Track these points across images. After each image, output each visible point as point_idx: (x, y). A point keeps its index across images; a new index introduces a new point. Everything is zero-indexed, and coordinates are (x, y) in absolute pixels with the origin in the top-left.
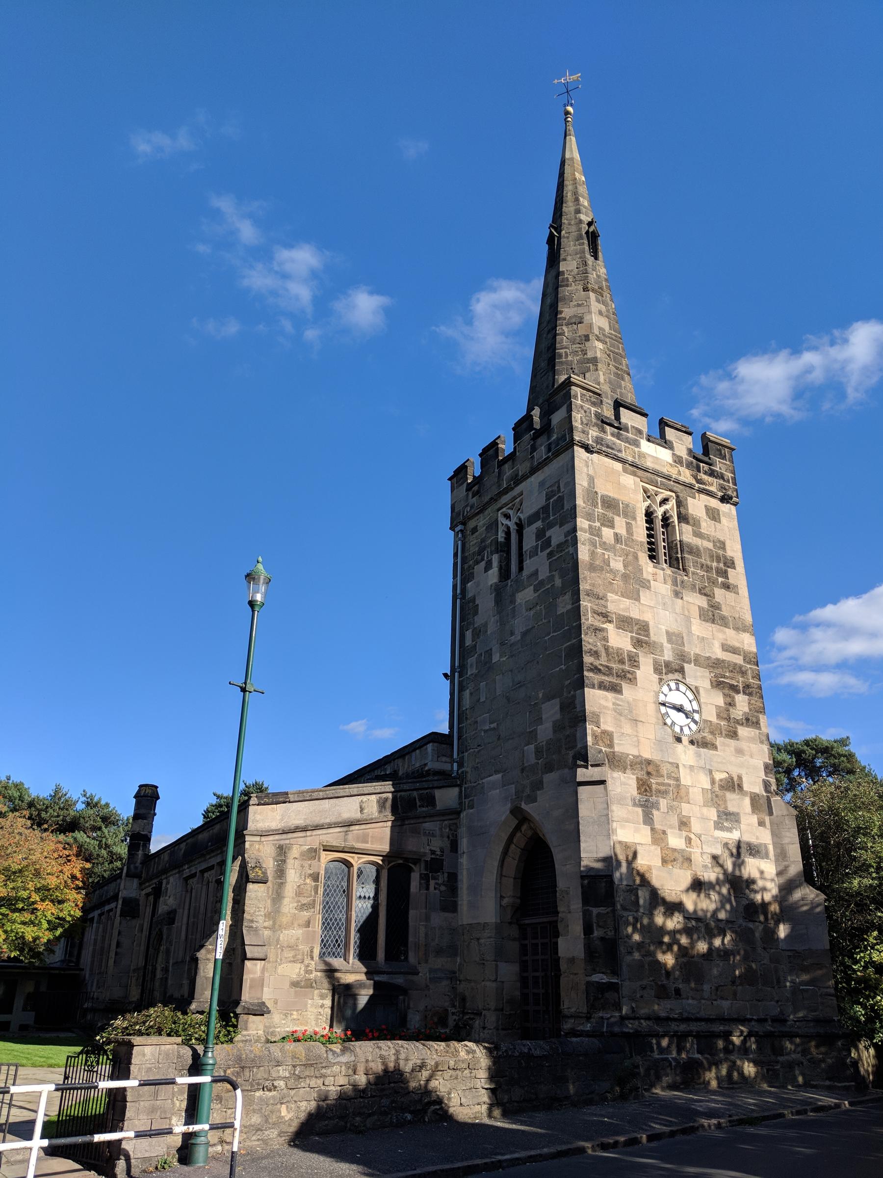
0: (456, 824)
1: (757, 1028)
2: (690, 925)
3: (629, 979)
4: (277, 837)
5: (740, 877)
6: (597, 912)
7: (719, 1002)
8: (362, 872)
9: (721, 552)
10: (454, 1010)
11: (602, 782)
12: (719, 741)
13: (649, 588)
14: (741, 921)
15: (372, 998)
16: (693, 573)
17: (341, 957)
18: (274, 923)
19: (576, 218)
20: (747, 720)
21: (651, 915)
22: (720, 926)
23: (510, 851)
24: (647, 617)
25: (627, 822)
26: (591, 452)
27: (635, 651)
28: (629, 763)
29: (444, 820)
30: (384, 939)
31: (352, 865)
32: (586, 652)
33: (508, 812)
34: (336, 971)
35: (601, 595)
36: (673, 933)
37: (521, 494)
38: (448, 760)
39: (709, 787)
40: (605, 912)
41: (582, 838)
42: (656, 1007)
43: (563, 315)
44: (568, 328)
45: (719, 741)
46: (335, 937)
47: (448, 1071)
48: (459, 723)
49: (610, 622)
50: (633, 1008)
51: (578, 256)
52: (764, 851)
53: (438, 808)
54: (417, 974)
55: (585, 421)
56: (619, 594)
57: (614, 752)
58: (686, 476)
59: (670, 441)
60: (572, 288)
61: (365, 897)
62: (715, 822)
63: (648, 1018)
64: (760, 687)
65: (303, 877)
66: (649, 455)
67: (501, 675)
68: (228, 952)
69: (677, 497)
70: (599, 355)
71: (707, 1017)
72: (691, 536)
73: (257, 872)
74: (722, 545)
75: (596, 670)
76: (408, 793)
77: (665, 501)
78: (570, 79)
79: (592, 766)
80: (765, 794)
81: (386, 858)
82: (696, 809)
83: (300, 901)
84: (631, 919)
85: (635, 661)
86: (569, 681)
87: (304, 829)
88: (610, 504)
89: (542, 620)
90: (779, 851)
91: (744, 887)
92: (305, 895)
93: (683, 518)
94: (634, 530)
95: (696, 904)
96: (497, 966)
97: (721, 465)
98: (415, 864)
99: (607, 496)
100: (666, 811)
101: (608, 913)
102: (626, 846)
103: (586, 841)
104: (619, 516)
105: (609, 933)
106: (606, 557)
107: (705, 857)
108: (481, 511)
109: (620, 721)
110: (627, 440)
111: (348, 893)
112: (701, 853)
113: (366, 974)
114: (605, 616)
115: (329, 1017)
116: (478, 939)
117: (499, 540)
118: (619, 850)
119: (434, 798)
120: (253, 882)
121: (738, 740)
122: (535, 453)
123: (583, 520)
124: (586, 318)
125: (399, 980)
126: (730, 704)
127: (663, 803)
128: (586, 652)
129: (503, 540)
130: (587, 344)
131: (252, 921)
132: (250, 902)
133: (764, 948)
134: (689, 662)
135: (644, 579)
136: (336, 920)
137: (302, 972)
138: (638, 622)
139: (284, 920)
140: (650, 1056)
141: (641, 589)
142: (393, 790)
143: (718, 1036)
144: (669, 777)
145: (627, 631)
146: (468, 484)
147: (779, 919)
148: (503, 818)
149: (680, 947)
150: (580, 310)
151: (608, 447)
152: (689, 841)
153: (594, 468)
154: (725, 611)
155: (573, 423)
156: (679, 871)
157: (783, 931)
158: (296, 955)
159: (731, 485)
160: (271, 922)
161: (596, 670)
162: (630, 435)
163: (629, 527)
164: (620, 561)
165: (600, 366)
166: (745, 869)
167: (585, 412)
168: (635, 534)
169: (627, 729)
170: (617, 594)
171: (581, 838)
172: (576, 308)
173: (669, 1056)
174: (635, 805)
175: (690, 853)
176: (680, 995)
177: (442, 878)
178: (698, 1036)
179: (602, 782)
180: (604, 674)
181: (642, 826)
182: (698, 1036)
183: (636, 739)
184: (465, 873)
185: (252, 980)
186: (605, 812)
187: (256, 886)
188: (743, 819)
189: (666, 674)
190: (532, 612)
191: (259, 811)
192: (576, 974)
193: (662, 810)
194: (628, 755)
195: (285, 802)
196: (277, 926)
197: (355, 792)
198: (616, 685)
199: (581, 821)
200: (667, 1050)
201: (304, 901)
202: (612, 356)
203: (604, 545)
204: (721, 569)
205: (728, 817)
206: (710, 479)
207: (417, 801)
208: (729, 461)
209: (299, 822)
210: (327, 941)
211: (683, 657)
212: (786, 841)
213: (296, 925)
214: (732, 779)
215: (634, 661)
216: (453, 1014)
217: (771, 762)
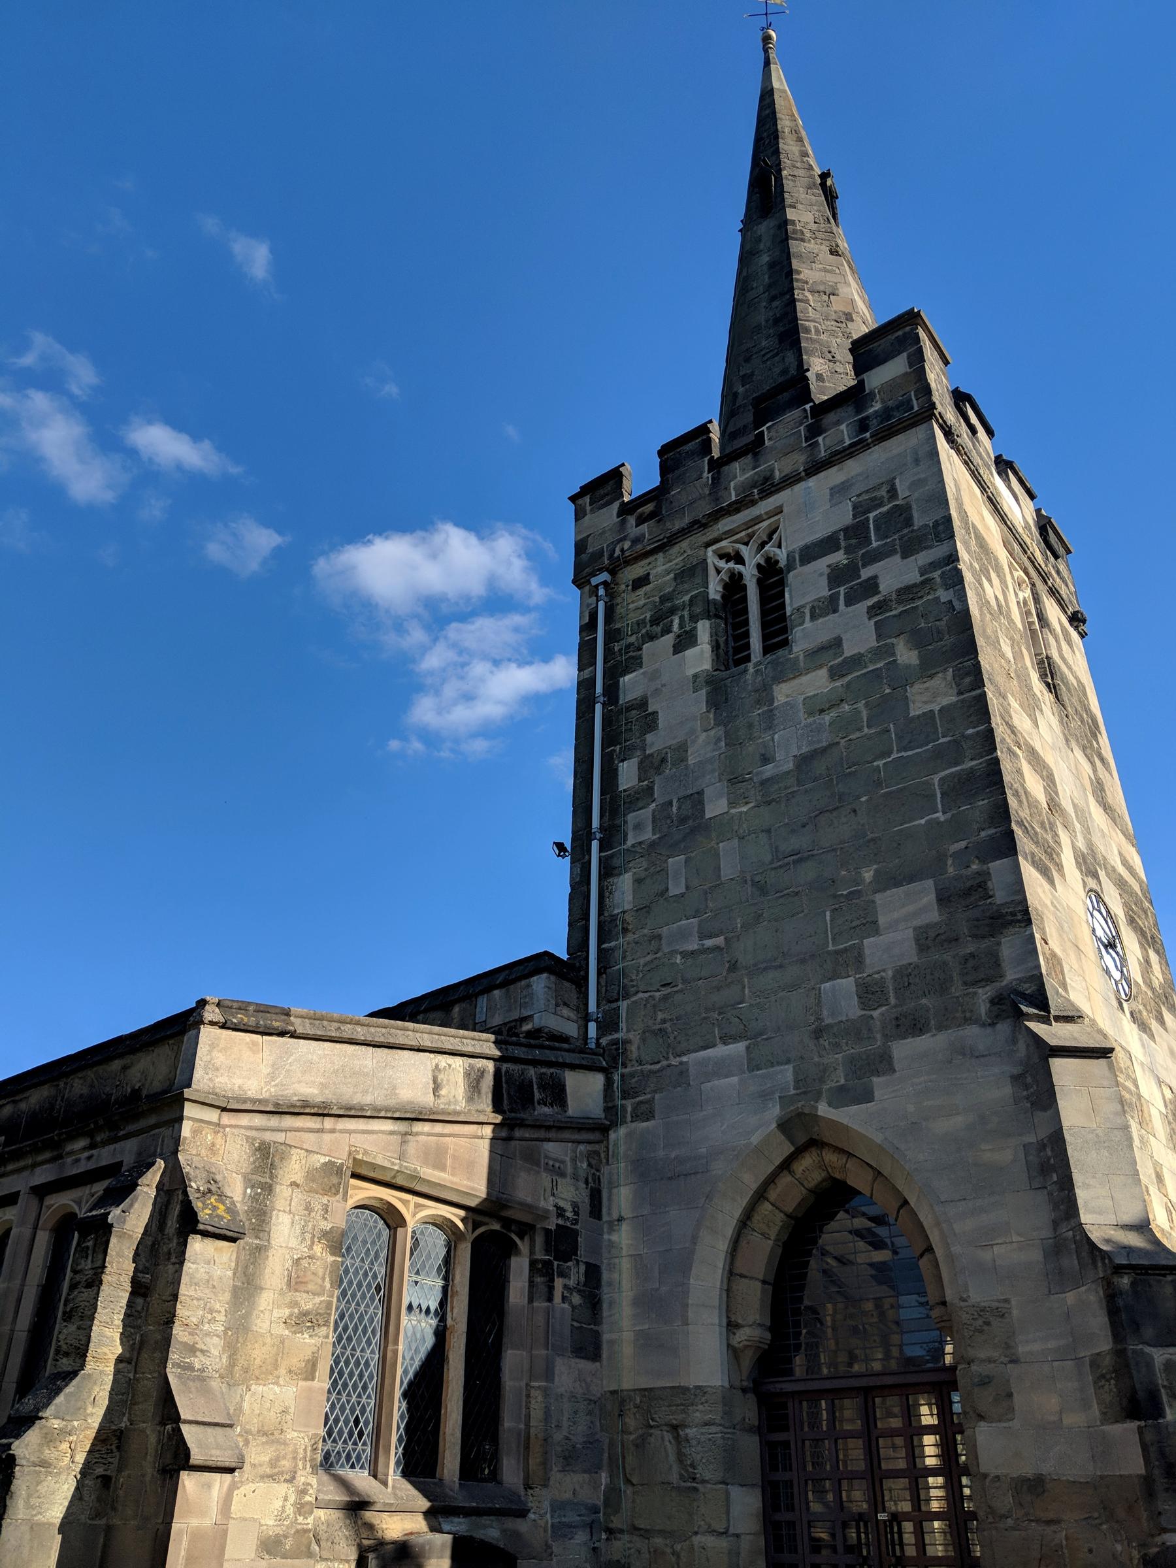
4: (258, 1120)
23: (756, 1217)
29: (579, 1142)
30: (460, 1422)
31: (402, 1222)
33: (774, 1125)
37: (779, 511)
41: (1077, 1177)
43: (801, 276)
46: (353, 1410)
48: (600, 941)
53: (570, 1112)
65: (308, 1236)
67: (736, 841)
68: (104, 1441)
73: (215, 1208)
79: (1058, 1019)
81: (475, 1214)
83: (295, 1304)
86: (963, 844)
87: (322, 1112)
89: (860, 729)
92: (311, 1287)
103: (1087, 1186)
108: (661, 548)
111: (387, 1292)
113: (428, 1514)
120: (205, 1234)
122: (820, 439)
129: (718, 597)
136: (357, 1363)
137: (290, 1510)
139: (258, 1353)
146: (623, 504)
148: (755, 1139)
158: (278, 1459)
177: (576, 1274)
184: (626, 1265)
185: (197, 1536)
186: (1119, 1121)
190: (827, 718)
191: (222, 1044)
192: (1049, 1522)
195: (282, 1034)
197: (426, 1041)
207: (536, 1091)
209: (307, 1089)
210: (337, 1420)
213: (282, 1371)
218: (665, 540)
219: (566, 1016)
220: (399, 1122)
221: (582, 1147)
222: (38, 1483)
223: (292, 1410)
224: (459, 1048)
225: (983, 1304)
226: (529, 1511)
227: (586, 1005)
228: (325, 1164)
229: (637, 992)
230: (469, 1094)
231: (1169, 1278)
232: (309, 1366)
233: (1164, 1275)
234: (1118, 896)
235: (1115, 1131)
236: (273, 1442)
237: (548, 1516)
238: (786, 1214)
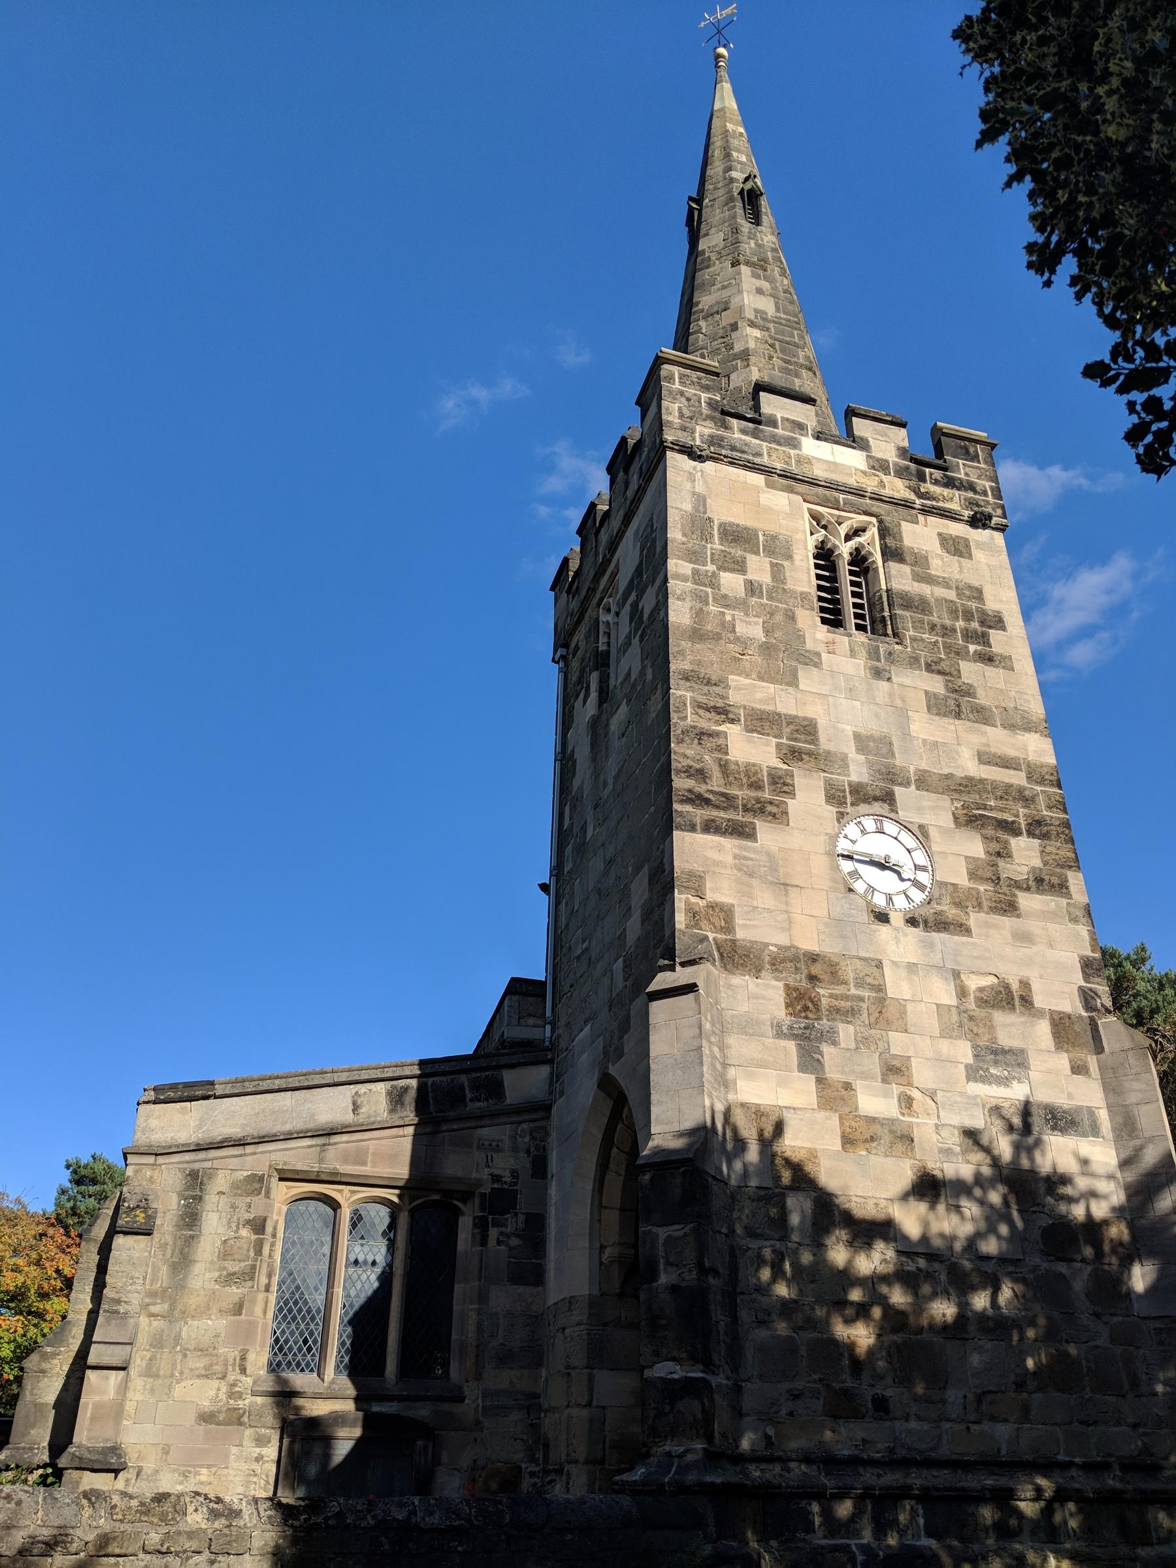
1: (1081, 1481)
2: (911, 1267)
3: (761, 1377)
4: (188, 1157)
5: (1033, 1172)
6: (664, 1236)
7: (986, 1426)
8: (360, 1218)
9: (973, 605)
10: (533, 1468)
11: (691, 988)
12: (974, 919)
13: (818, 665)
14: (1036, 1260)
15: (359, 1442)
16: (913, 639)
17: (312, 1370)
18: (172, 1308)
19: (725, 179)
20: (1039, 881)
21: (819, 1246)
22: (985, 1268)
24: (813, 711)
25: (761, 1066)
26: (700, 458)
27: (785, 767)
28: (767, 958)
29: (521, 1122)
32: (678, 772)
34: (294, 1394)
35: (714, 678)
36: (872, 1283)
38: (539, 1022)
39: (954, 1001)
40: (681, 1233)
41: (654, 1097)
42: (828, 1435)
44: (706, 321)
45: (974, 919)
46: (301, 1334)
47: (141, 1556)
49: (732, 721)
50: (767, 1437)
51: (726, 224)
52: (1087, 1122)
53: (508, 1101)
54: (461, 1399)
55: (686, 412)
56: (754, 676)
57: (734, 941)
58: (897, 488)
59: (862, 439)
60: (715, 268)
61: (365, 1262)
62: (967, 1067)
63: (807, 1460)
64: (1067, 824)
65: (234, 1225)
66: (819, 460)
69: (880, 522)
70: (752, 345)
71: (954, 1457)
72: (910, 581)
73: (136, 1216)
74: (978, 594)
75: (700, 800)
76: (449, 1078)
77: (858, 532)
78: (721, 15)
79: (683, 964)
80: (1085, 1014)
81: (408, 1189)
82: (924, 1044)
83: (225, 1268)
84: (767, 1253)
85: (784, 784)
87: (240, 1143)
88: (736, 536)
90: (1121, 1120)
91: (1042, 1190)
92: (236, 1257)
93: (892, 553)
94: (788, 574)
95: (926, 1224)
96: (591, 1378)
97: (967, 469)
98: (464, 1201)
99: (731, 524)
100: (853, 1046)
101: (685, 1234)
102: (759, 1113)
104: (757, 553)
105: (687, 1276)
106: (728, 618)
107: (945, 1133)
109: (750, 886)
110: (774, 439)
112: (937, 1126)
113: (357, 1400)
114: (724, 713)
115: (272, 1480)
116: (564, 1329)
117: (600, 649)
118: (739, 1118)
119: (500, 1084)
120: (125, 1233)
121: (1018, 916)
123: (680, 562)
124: (735, 302)
125: (423, 1412)
126: (999, 854)
127: (846, 1032)
128: (678, 772)
130: (734, 335)
131: (118, 1302)
132: (117, 1268)
133: (1097, 1315)
134: (907, 784)
135: (808, 651)
137: (223, 1396)
138: (791, 720)
140: (804, 1540)
141: (800, 666)
142: (418, 1072)
143: (980, 1498)
144: (859, 984)
145: (768, 735)
147: (1129, 1255)
149: (888, 1308)
150: (725, 294)
151: (733, 448)
152: (907, 1102)
153: (706, 482)
154: (983, 698)
155: (664, 417)
156: (882, 1159)
157: (1140, 1278)
158: (211, 1365)
159: (990, 499)
160: (166, 1306)
161: (700, 800)
162: (780, 431)
163: (777, 572)
164: (756, 624)
165: (753, 359)
166: (1043, 1154)
167: (688, 400)
168: (789, 581)
169: (765, 898)
170: (748, 676)
171: (652, 1097)
172: (720, 293)
173: (853, 1542)
174: (780, 1034)
175: (910, 1125)
176: (887, 1411)
177: (513, 1223)
178: (926, 1498)
179: (691, 988)
180: (717, 807)
181: (797, 1074)
182: (926, 1498)
183: (784, 916)
185: (98, 1406)
186: (696, 1044)
187: (131, 1239)
188: (1035, 1061)
189: (852, 804)
193: (842, 1046)
194: (766, 945)
196: (177, 1313)
198: (743, 825)
199: (652, 1066)
200: (849, 1527)
201: (234, 1267)
202: (777, 346)
203: (724, 601)
204: (976, 632)
205: (1000, 1057)
206: (946, 492)
208: (986, 462)
209: (233, 1130)
210: (286, 1341)
211: (892, 776)
212: (1132, 1098)
213: (214, 1311)
214: (1007, 987)
215: (782, 784)
216: (532, 1474)
217: (1097, 955)
220: (315, 1139)
221: (525, 1126)
222: (38, 1382)
223: (223, 1335)
224: (357, 1078)
226: (465, 1398)
228: (248, 1176)
230: (390, 1107)
232: (237, 1307)
235: (691, 1053)
236: (207, 1355)
237: (480, 1400)
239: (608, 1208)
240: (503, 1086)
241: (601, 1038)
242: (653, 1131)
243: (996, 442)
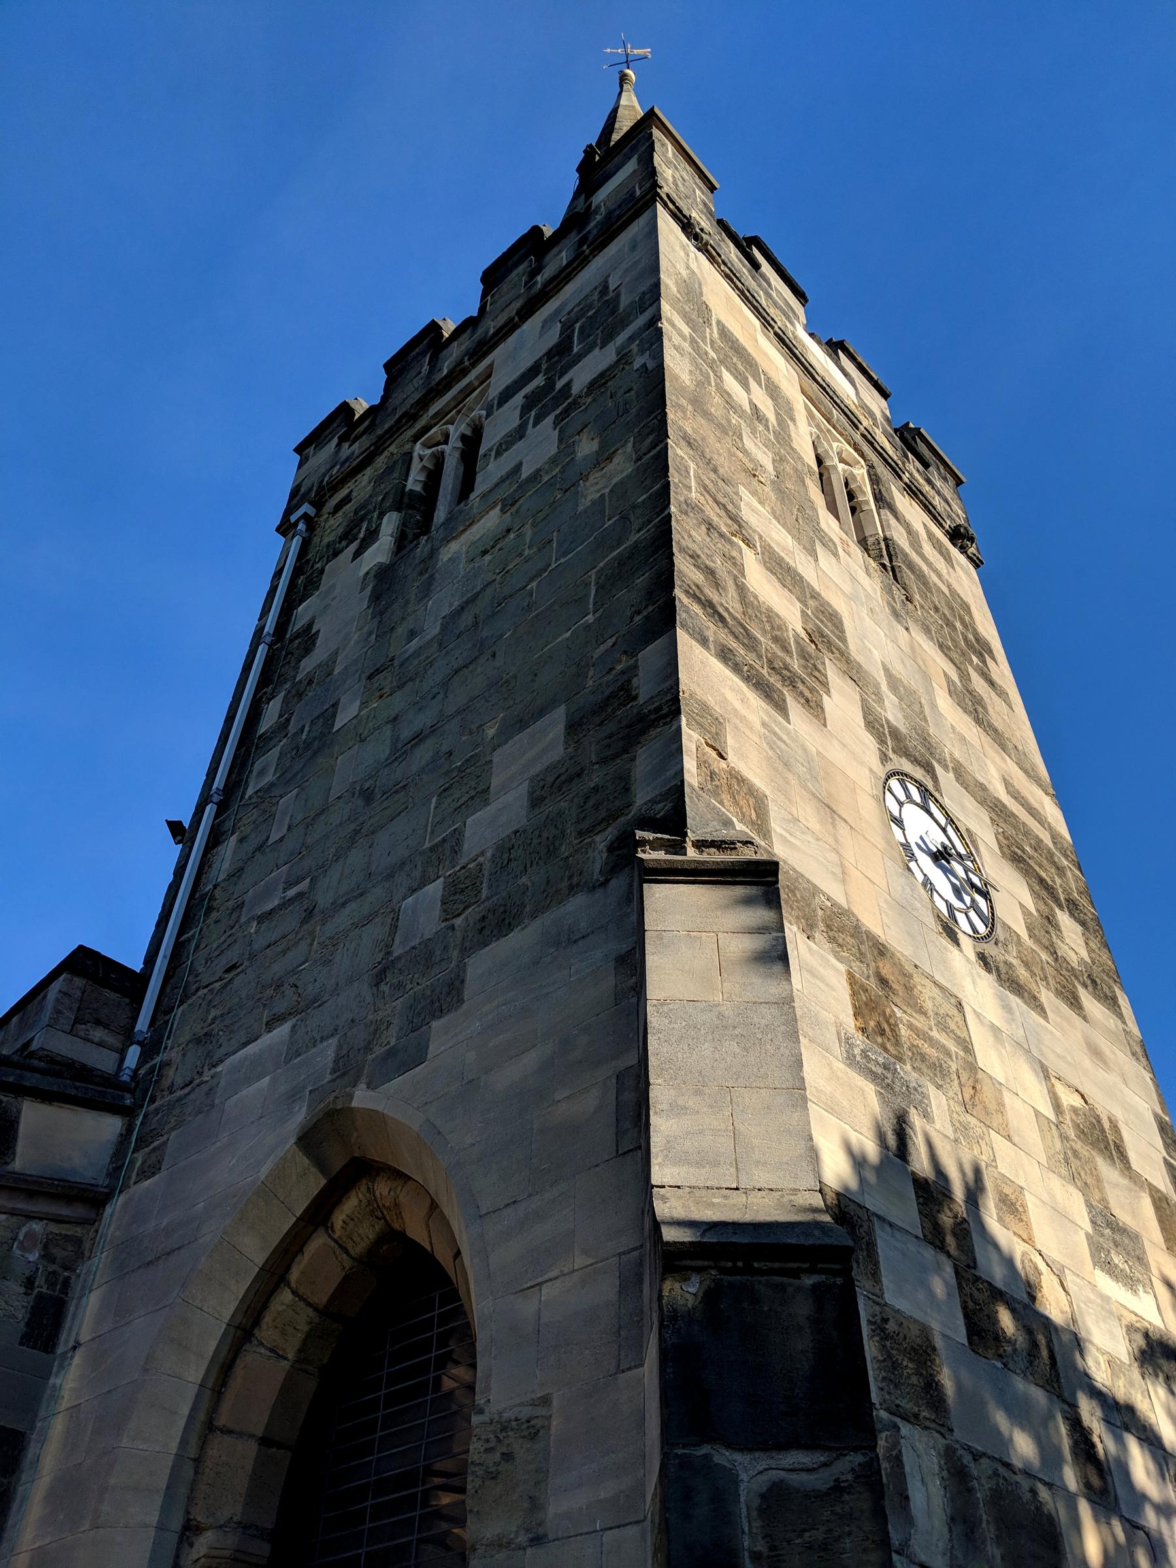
0: (78, 1242)
6: (762, 1483)
29: (30, 1217)
33: (292, 1141)
40: (819, 1481)
41: (660, 1092)
53: (18, 1165)
101: (838, 1488)
103: (677, 1110)
129: (418, 488)
218: (372, 448)
219: (96, 1040)
221: (37, 1227)
225: (506, 1415)
227: (135, 1019)
229: (197, 990)
231: (808, 1281)
233: (795, 1274)
234: (988, 821)
235: (764, 1009)
238: (316, 1310)
239: (230, 1432)
240: (16, 1131)
241: (333, 1042)
242: (655, 1179)
243: (964, 479)
